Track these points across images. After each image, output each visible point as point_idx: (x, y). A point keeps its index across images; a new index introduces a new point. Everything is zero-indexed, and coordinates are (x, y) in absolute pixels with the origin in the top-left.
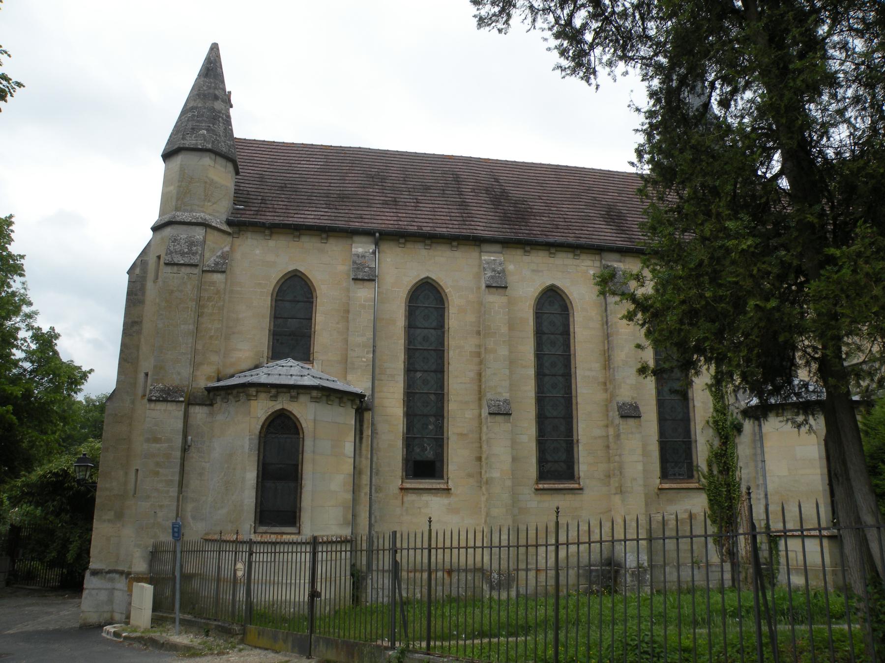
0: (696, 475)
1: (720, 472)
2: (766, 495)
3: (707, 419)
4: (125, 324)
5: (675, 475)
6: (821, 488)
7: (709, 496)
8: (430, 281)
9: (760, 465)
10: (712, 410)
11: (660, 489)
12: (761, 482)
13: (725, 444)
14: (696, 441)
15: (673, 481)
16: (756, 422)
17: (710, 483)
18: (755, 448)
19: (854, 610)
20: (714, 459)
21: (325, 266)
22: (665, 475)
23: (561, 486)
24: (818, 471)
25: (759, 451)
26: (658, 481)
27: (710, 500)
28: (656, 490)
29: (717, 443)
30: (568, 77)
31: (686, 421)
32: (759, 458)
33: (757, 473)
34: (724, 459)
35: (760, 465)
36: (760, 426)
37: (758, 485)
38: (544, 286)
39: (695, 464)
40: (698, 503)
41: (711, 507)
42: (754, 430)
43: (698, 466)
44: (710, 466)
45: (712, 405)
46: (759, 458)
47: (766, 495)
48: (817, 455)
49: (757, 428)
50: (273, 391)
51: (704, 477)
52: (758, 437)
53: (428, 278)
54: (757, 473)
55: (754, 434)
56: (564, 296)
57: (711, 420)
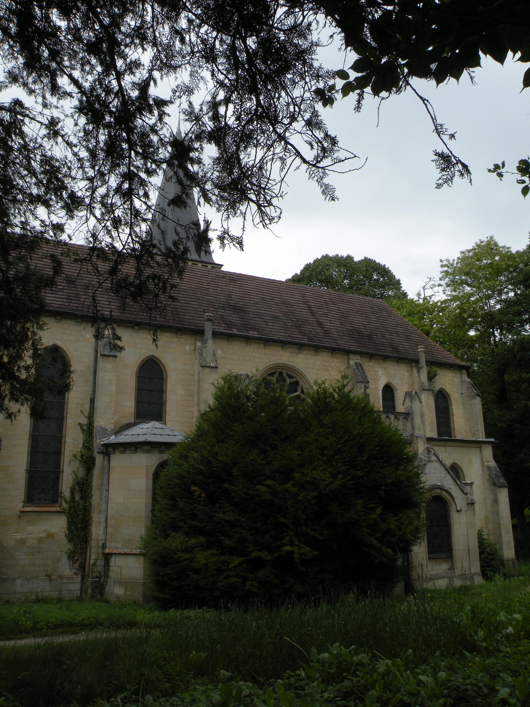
0: (59, 501)
1: (81, 498)
2: (107, 519)
3: (75, 453)
4: (484, 413)
5: (40, 499)
6: (144, 515)
7: (68, 519)
8: (154, 359)
9: (105, 493)
10: (81, 446)
11: (22, 512)
12: (104, 507)
13: (87, 475)
14: (63, 471)
15: (39, 505)
16: (106, 458)
17: (70, 508)
18: (102, 479)
19: (28, 615)
20: (77, 487)
21: (176, 355)
22: (29, 499)
23: (45, 509)
24: (144, 500)
25: (105, 482)
26: (21, 505)
27: (69, 522)
28: (18, 513)
29: (81, 473)
30: (471, 176)
31: (57, 454)
32: (105, 487)
33: (101, 500)
34: (83, 487)
35: (105, 493)
36: (109, 461)
37: (100, 511)
38: (144, 357)
39: (60, 490)
40: (58, 525)
41: (69, 528)
42: (103, 464)
43: (62, 493)
44: (73, 493)
45: (81, 441)
46: (105, 487)
47: (107, 519)
48: (144, 487)
49: (106, 463)
50: (163, 448)
51: (66, 502)
52: (106, 470)
53: (152, 356)
54: (101, 500)
55: (103, 468)
56: (161, 365)
57: (79, 455)
